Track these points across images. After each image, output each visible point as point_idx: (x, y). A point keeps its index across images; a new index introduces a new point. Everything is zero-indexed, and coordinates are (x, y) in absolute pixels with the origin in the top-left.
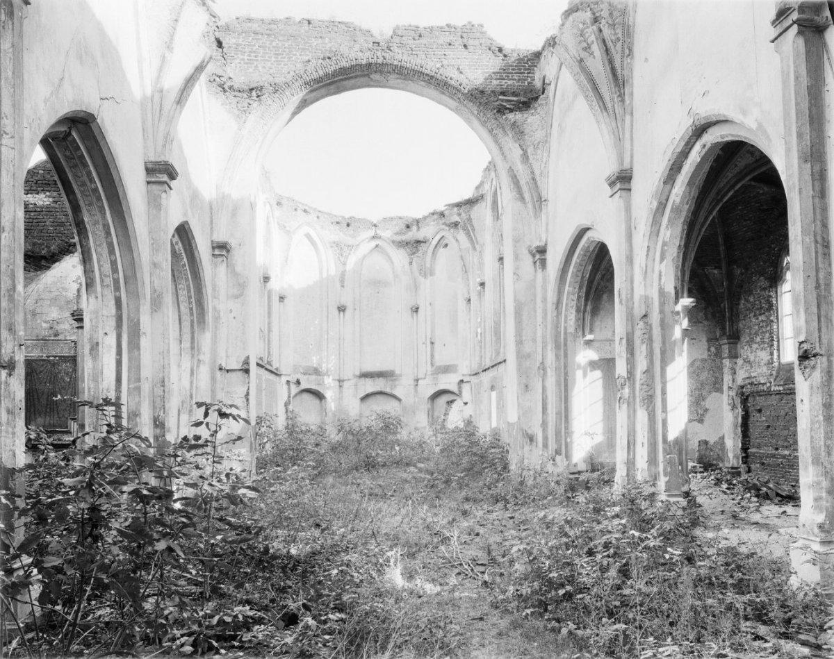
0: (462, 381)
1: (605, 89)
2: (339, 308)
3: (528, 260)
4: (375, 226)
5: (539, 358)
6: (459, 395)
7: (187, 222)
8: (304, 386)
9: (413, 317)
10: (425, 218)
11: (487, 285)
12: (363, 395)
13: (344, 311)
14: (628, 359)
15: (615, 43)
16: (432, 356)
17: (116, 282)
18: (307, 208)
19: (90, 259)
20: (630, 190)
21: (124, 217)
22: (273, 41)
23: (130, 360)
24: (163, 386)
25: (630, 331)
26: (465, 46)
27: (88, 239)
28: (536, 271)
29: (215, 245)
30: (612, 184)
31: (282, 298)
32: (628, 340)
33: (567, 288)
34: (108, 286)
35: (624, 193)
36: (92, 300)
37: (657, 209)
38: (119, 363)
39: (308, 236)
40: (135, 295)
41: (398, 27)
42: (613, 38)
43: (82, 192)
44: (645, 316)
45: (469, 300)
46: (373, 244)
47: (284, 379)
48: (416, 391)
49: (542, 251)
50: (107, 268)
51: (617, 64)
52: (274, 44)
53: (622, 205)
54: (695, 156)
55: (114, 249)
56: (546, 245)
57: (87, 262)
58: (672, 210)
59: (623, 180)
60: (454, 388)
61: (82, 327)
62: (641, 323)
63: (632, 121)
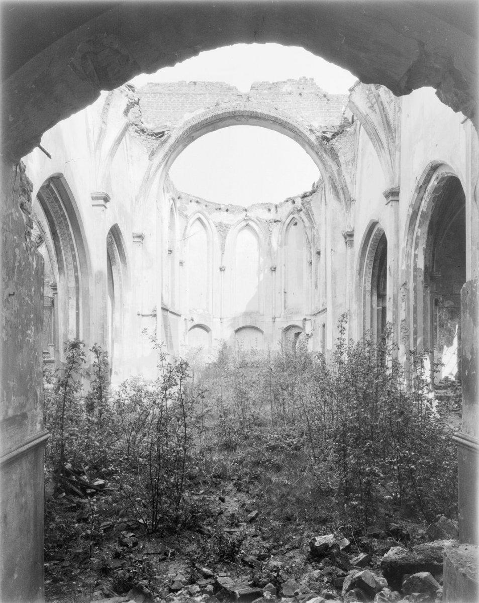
0: (305, 319)
1: (382, 135)
2: (220, 269)
3: (342, 241)
4: (246, 210)
5: (347, 307)
6: (304, 329)
7: (117, 224)
8: (196, 322)
9: (272, 274)
10: (281, 204)
11: (321, 253)
12: (236, 328)
13: (224, 270)
14: (393, 312)
15: (389, 103)
16: (285, 302)
17: (75, 267)
18: (199, 200)
19: (59, 241)
20: (398, 201)
21: (79, 228)
22: (171, 98)
23: (84, 312)
24: (103, 328)
25: (396, 293)
26: (300, 94)
27: (59, 242)
28: (347, 248)
29: (135, 235)
30: (387, 196)
31: (181, 263)
32: (394, 299)
33: (366, 260)
34: (70, 270)
35: (394, 203)
36: (62, 277)
37: (412, 216)
38: (78, 315)
39: (199, 219)
40: (86, 273)
41: (253, 84)
42: (388, 100)
43: (56, 216)
44: (405, 284)
45: (311, 263)
46: (244, 223)
47: (183, 317)
48: (274, 326)
49: (351, 235)
50: (70, 259)
51: (391, 117)
52: (172, 100)
53: (392, 210)
54: (433, 182)
55: (74, 248)
56: (353, 231)
57: (59, 255)
58: (422, 216)
59: (393, 194)
60: (300, 324)
61: (56, 293)
62: (402, 289)
63: (400, 156)
